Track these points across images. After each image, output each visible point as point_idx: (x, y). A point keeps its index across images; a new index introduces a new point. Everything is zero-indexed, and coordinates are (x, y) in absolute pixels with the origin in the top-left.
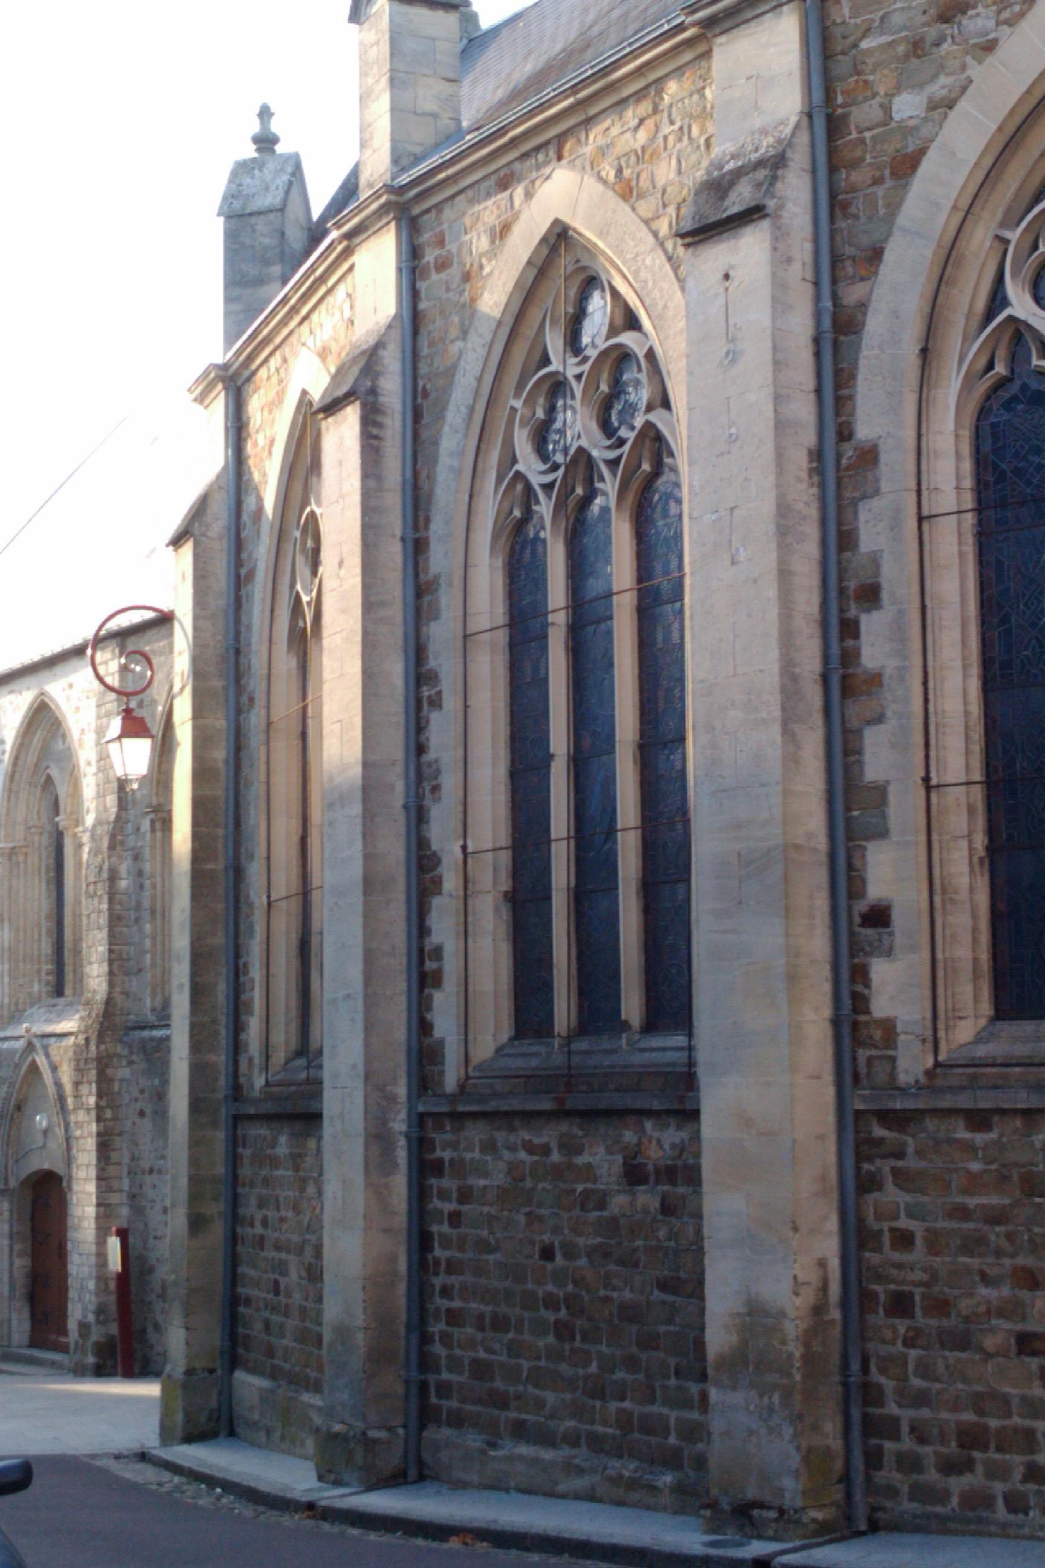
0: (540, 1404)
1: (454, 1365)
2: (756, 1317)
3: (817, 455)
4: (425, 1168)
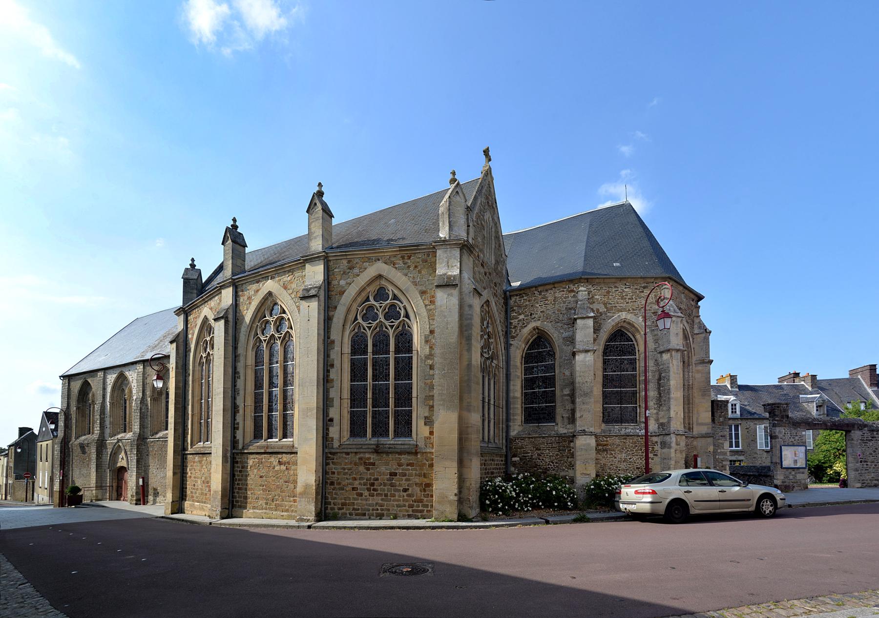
3: (324, 340)
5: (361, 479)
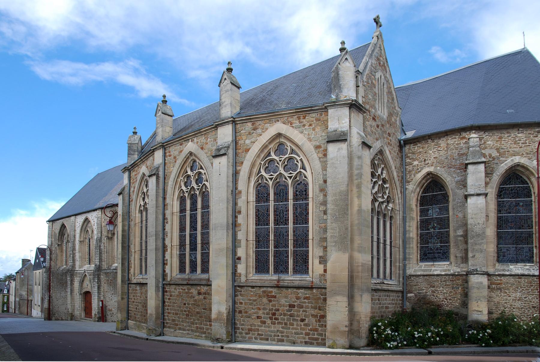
0: (183, 325)
1: (169, 319)
2: (219, 313)
3: (232, 191)
4: (164, 291)
5: (264, 309)
